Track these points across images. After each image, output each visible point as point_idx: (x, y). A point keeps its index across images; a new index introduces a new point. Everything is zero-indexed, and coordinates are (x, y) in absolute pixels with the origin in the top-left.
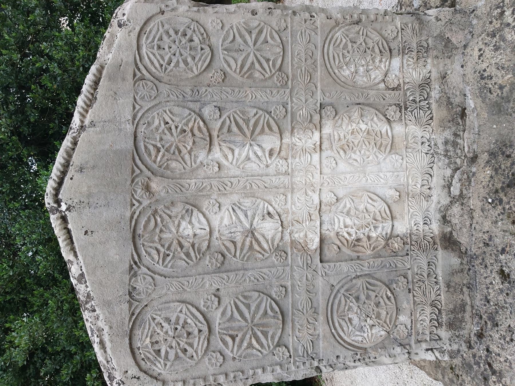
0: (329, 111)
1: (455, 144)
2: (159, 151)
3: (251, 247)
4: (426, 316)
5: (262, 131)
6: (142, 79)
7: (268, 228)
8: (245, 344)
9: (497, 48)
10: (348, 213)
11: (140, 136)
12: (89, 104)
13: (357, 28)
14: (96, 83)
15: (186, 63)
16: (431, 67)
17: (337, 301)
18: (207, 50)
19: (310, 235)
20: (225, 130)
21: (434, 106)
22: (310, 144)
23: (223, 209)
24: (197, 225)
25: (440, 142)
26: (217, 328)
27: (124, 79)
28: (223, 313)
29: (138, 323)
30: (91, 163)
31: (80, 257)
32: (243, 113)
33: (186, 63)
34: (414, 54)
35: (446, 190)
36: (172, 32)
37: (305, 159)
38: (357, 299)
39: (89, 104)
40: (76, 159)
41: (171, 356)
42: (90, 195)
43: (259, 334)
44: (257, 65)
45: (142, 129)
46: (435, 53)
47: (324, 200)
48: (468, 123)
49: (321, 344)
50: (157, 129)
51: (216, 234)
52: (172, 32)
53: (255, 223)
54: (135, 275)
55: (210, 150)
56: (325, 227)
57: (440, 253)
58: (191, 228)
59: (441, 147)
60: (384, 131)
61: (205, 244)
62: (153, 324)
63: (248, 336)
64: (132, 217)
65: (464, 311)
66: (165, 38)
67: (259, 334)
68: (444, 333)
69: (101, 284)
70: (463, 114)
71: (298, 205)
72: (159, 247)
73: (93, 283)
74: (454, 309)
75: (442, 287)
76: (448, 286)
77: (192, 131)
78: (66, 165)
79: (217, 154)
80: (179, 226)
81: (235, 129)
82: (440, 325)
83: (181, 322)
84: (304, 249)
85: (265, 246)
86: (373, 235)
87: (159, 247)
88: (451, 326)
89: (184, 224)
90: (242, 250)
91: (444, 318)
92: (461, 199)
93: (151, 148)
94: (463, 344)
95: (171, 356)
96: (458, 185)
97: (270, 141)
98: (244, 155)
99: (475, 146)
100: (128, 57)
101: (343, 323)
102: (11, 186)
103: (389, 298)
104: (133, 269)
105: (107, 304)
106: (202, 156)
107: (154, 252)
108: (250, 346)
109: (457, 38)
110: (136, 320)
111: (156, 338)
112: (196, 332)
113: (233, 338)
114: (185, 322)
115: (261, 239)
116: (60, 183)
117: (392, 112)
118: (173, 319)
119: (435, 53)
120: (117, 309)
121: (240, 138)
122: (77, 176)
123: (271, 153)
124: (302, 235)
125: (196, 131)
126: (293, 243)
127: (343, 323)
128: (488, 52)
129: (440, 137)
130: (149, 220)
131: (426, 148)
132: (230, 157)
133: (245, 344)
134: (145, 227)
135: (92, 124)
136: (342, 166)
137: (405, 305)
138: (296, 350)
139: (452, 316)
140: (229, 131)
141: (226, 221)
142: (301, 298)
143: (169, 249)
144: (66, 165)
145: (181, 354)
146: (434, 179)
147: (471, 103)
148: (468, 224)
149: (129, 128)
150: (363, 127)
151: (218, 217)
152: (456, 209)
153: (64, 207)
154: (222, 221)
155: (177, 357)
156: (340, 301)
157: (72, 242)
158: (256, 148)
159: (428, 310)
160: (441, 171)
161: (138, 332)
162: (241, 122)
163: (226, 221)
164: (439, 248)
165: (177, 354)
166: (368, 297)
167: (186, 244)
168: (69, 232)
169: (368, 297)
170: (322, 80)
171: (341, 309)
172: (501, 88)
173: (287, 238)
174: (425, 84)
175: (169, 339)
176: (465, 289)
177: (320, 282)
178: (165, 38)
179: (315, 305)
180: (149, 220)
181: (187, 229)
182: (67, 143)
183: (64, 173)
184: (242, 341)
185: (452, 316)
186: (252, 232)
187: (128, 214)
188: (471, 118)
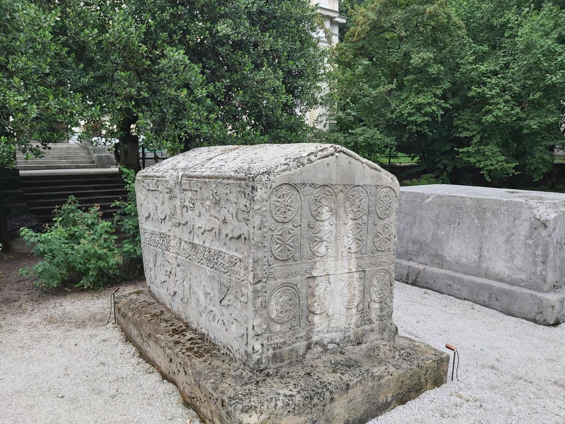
0: (362, 275)
1: (348, 342)
2: (353, 196)
3: (316, 241)
4: (278, 340)
5: (357, 243)
6: (377, 189)
7: (322, 249)
8: (278, 241)
9: (390, 350)
10: (325, 290)
11: (358, 187)
12: (369, 166)
13: (389, 285)
14: (376, 169)
15: (381, 207)
16: (376, 324)
17: (290, 288)
18: (384, 217)
19: (318, 271)
20: (359, 226)
21: (362, 327)
22: (352, 267)
23: (330, 226)
24: (326, 214)
25: (349, 333)
26: (286, 226)
27: (377, 181)
28: (291, 229)
29: (291, 187)
30: (351, 167)
31: (319, 161)
32: (364, 234)
33: (381, 207)
34: (380, 314)
35: (330, 341)
36: (390, 201)
37: (346, 265)
38: (290, 300)
39: (369, 166)
40: (353, 160)
41: (277, 204)
42: (341, 166)
43: (281, 248)
44: (379, 239)
45: (360, 188)
46: (381, 324)
47: (330, 276)
48: (356, 347)
49: (273, 282)
50: (360, 195)
51: (321, 224)
52: (390, 201)
53: (324, 242)
54: (311, 186)
55: (352, 219)
56: (320, 278)
57: (305, 343)
58: (325, 213)
59: (347, 335)
60: (354, 303)
61: (318, 218)
62: (291, 195)
63: (281, 242)
64: (331, 184)
65: (280, 362)
66: (389, 198)
67: (281, 248)
68: (271, 352)
69: (310, 170)
70: (359, 344)
71: (330, 264)
72: (320, 197)
73: (310, 167)
74: (282, 356)
75: (291, 347)
76: (292, 350)
77: (359, 211)
78: (350, 156)
79: (350, 222)
80: (327, 206)
81: (359, 230)
82: (274, 349)
83: (290, 208)
84: (313, 268)
85: (315, 248)
86: (316, 304)
87: (320, 197)
88: (274, 355)
89: (327, 208)
90: (315, 237)
91: (278, 351)
92: (325, 350)
93: (354, 193)
94: (265, 365)
95: (277, 204)
96: (332, 347)
97: (354, 248)
98: (349, 235)
99: (347, 352)
100: (384, 183)
101: (280, 293)
102: (167, 20)
103: (288, 318)
104: (312, 185)
105: (301, 174)
106: (351, 216)
107: (318, 195)
108: (277, 243)
109: (386, 335)
110: (293, 186)
111: (285, 196)
112: (285, 216)
113: (281, 235)
114: (290, 210)
115: (318, 246)
116: (345, 153)
117: (361, 306)
118: (291, 204)
119: (381, 324)
120: (299, 178)
121: (355, 233)
122: (347, 161)
123: (350, 248)
124: (318, 267)
125: (359, 213)
126: (315, 262)
127: (280, 293)
128: (387, 347)
129: (351, 333)
130: (330, 192)
131: (347, 326)
132: (349, 229)
133: (278, 241)
134: (328, 190)
135: (364, 167)
136: (342, 284)
137: (284, 327)
138: (272, 268)
139: (278, 355)
140: (358, 228)
141: (326, 228)
142: (293, 269)
143: (319, 202)
144: (350, 156)
145: (278, 209)
146: (335, 333)
147: (363, 346)
148: (315, 357)
149: (361, 184)
150: (356, 293)
151: (328, 224)
152: (320, 349)
153: (337, 154)
154: (326, 228)
155: (277, 206)
156: (290, 290)
157: (324, 157)
158: (352, 241)
159: (282, 340)
160: (337, 336)
161: (288, 187)
162: (361, 233)
163: (326, 228)
164: (307, 342)
165: (278, 206)
166: (290, 305)
167: (319, 210)
168: (328, 156)
169: (290, 305)
170: (373, 270)
171: (287, 291)
172: (378, 355)
173: (317, 259)
174: (370, 321)
175: (284, 203)
176: (290, 360)
177: (299, 278)
178: (389, 198)
179: (289, 276)
180: (330, 192)
181: (325, 210)
182: (358, 156)
183: (348, 155)
184: (279, 239)
185: (278, 355)
186: (322, 241)
187: (333, 183)
188: (358, 348)
